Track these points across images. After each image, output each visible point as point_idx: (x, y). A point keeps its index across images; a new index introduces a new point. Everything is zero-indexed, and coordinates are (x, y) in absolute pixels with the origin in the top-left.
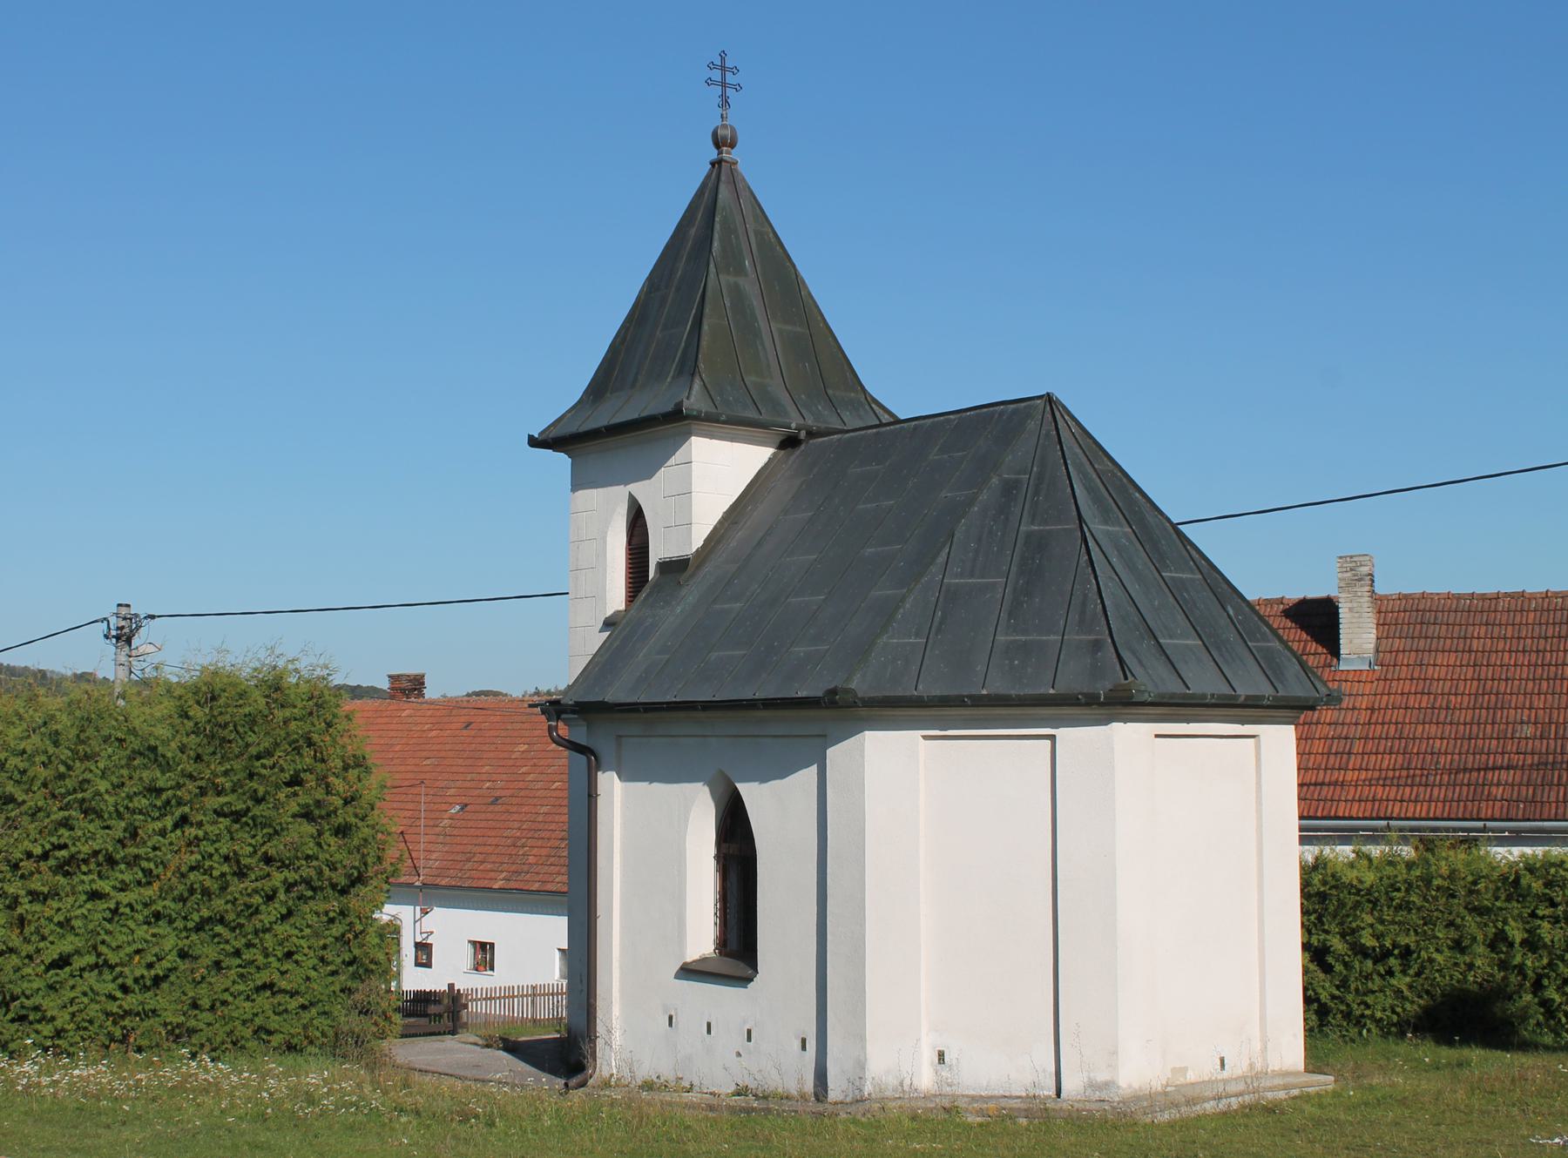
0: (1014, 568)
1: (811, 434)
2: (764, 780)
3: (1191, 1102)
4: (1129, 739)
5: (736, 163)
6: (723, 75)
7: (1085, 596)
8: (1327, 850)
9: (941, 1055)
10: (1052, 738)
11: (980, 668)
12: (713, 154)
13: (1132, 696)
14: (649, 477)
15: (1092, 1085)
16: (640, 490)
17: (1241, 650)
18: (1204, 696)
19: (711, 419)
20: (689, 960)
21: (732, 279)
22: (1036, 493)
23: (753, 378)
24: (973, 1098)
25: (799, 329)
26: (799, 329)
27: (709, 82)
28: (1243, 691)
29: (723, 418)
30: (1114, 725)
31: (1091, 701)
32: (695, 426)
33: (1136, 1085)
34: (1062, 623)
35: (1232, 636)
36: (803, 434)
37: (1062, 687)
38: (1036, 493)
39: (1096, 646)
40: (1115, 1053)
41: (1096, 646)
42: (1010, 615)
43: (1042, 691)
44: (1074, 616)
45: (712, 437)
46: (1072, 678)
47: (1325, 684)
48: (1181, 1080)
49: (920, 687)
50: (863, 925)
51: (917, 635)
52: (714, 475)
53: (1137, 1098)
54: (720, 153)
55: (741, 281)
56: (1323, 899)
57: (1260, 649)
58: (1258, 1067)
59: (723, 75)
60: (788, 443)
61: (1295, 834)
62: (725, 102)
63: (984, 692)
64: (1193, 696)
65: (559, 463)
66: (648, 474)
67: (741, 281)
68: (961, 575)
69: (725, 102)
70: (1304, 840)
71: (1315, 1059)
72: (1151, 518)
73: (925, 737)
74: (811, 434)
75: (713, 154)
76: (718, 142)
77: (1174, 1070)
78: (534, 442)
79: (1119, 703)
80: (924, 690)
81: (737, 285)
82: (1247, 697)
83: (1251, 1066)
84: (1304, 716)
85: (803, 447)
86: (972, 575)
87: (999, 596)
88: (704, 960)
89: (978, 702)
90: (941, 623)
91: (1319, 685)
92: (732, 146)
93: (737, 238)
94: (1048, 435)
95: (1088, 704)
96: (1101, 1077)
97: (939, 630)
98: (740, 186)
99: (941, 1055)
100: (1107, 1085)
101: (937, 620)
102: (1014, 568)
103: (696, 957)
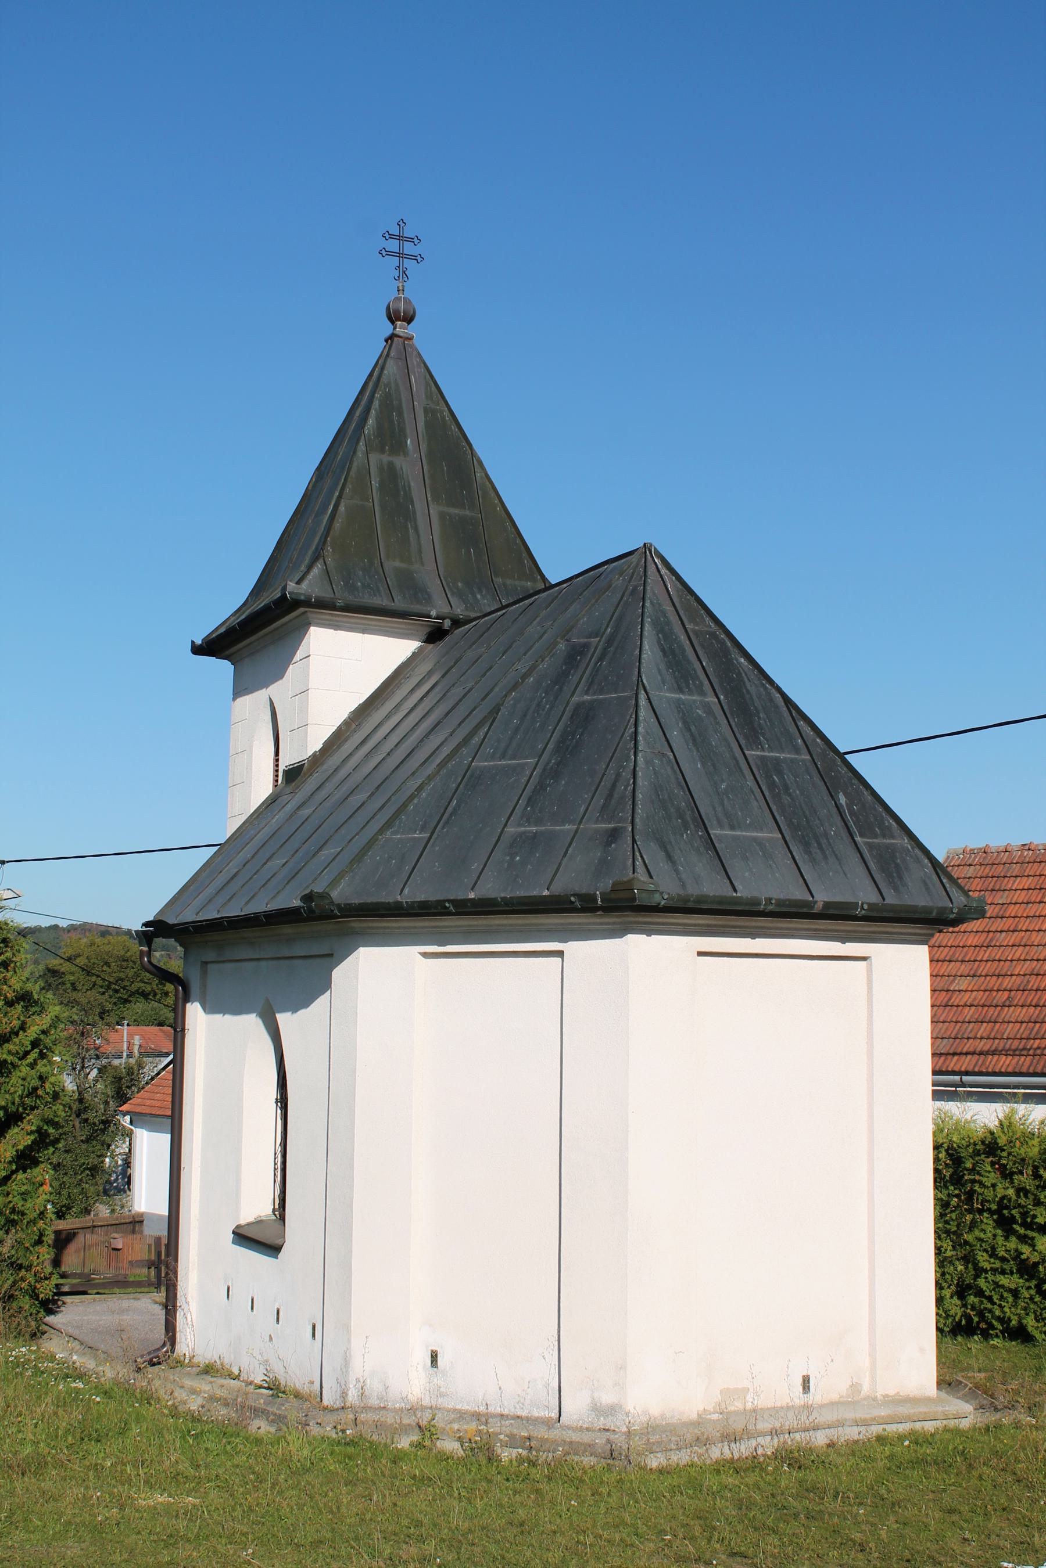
0: (551, 746)
1: (457, 623)
2: (295, 1010)
3: (731, 1438)
4: (653, 960)
5: (411, 339)
6: (401, 247)
7: (618, 775)
8: (1022, 1109)
9: (434, 1357)
10: (560, 954)
11: (476, 867)
12: (388, 329)
13: (634, 899)
14: (282, 678)
15: (596, 1409)
16: (275, 690)
17: (843, 847)
18: (756, 902)
19: (322, 605)
20: (243, 1222)
21: (386, 458)
22: (601, 659)
23: (397, 564)
24: (462, 1415)
25: (468, 513)
26: (468, 513)
27: (385, 253)
28: (822, 897)
29: (340, 603)
30: (631, 938)
31: (587, 905)
32: (312, 614)
33: (655, 1411)
34: (582, 809)
35: (835, 828)
36: (447, 624)
37: (559, 887)
38: (601, 659)
39: (614, 835)
40: (623, 1367)
41: (614, 835)
42: (530, 801)
43: (535, 893)
44: (599, 800)
45: (336, 627)
46: (572, 876)
47: (966, 893)
48: (738, 1405)
49: (406, 891)
50: (352, 1187)
51: (423, 829)
52: (344, 667)
53: (650, 1427)
54: (395, 328)
55: (399, 461)
56: (958, 1167)
57: (871, 847)
58: (866, 1389)
59: (401, 247)
60: (435, 636)
61: (929, 1089)
62: (403, 274)
63: (472, 896)
64: (738, 901)
65: (222, 669)
66: (279, 674)
67: (399, 461)
68: (492, 757)
69: (403, 274)
70: (937, 1096)
71: (947, 1382)
72: (752, 688)
73: (425, 955)
74: (457, 623)
75: (388, 329)
76: (393, 317)
77: (725, 1392)
78: (198, 650)
79: (622, 909)
80: (413, 893)
81: (391, 466)
82: (827, 905)
83: (855, 1387)
84: (946, 937)
85: (447, 639)
86: (503, 756)
87: (524, 780)
88: (259, 1222)
89: (485, 907)
90: (451, 815)
91: (954, 892)
92: (409, 319)
93: (400, 414)
94: (634, 591)
95: (584, 910)
96: (607, 1398)
97: (447, 822)
98: (414, 361)
99: (434, 1357)
100: (612, 1410)
101: (450, 809)
102: (551, 746)
103: (251, 1219)
